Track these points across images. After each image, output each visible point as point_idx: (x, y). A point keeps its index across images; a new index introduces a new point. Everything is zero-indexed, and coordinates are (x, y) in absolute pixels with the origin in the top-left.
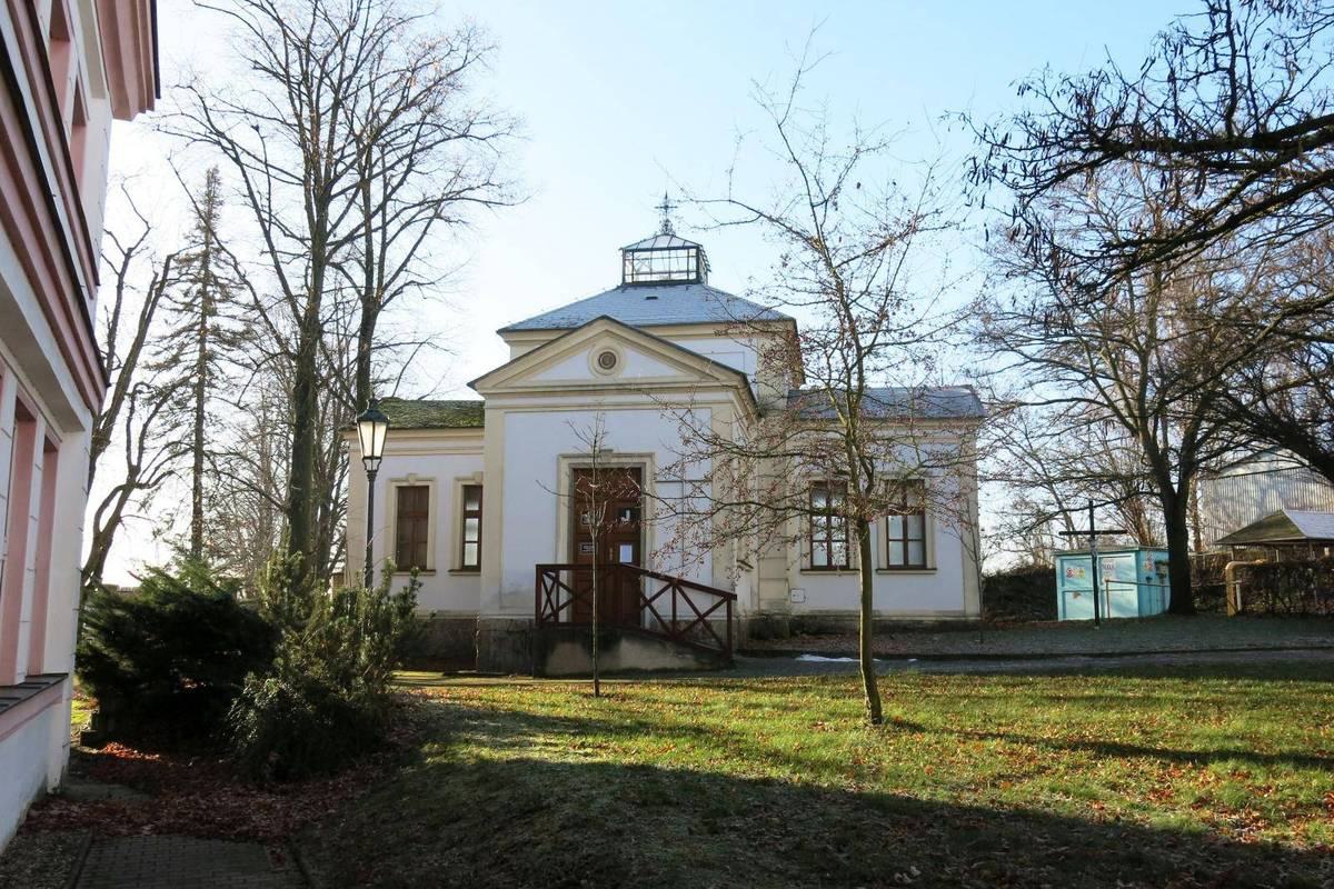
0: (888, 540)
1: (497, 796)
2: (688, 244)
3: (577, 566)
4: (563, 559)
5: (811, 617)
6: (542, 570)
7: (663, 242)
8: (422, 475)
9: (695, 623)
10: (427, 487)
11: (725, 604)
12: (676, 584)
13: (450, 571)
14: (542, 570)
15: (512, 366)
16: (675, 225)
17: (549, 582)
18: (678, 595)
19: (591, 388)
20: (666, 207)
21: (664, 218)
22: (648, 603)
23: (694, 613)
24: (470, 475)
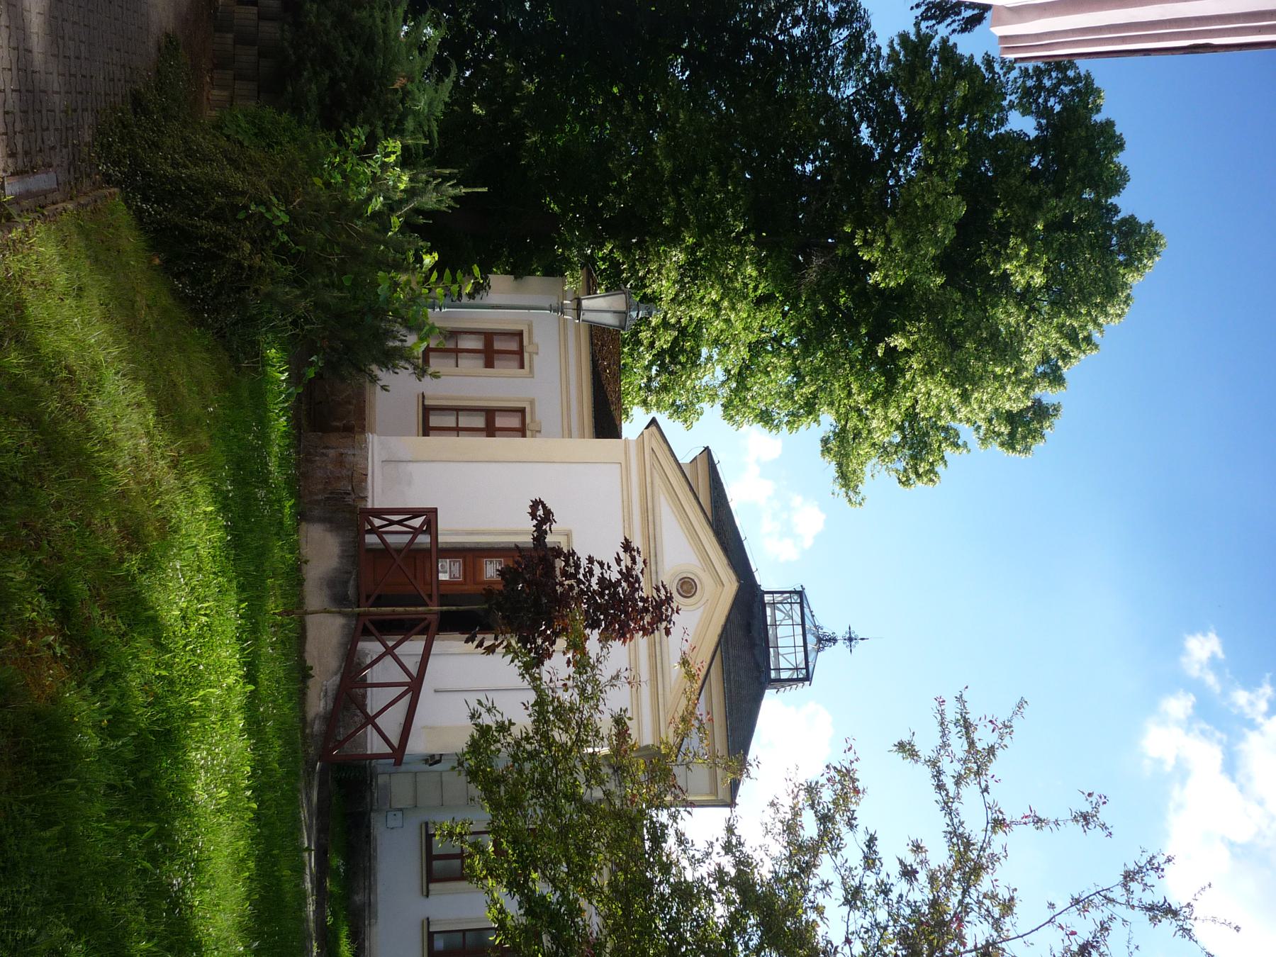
5: (368, 836)
7: (811, 640)
11: (389, 751)
12: (414, 686)
16: (829, 652)
17: (417, 522)
20: (850, 639)
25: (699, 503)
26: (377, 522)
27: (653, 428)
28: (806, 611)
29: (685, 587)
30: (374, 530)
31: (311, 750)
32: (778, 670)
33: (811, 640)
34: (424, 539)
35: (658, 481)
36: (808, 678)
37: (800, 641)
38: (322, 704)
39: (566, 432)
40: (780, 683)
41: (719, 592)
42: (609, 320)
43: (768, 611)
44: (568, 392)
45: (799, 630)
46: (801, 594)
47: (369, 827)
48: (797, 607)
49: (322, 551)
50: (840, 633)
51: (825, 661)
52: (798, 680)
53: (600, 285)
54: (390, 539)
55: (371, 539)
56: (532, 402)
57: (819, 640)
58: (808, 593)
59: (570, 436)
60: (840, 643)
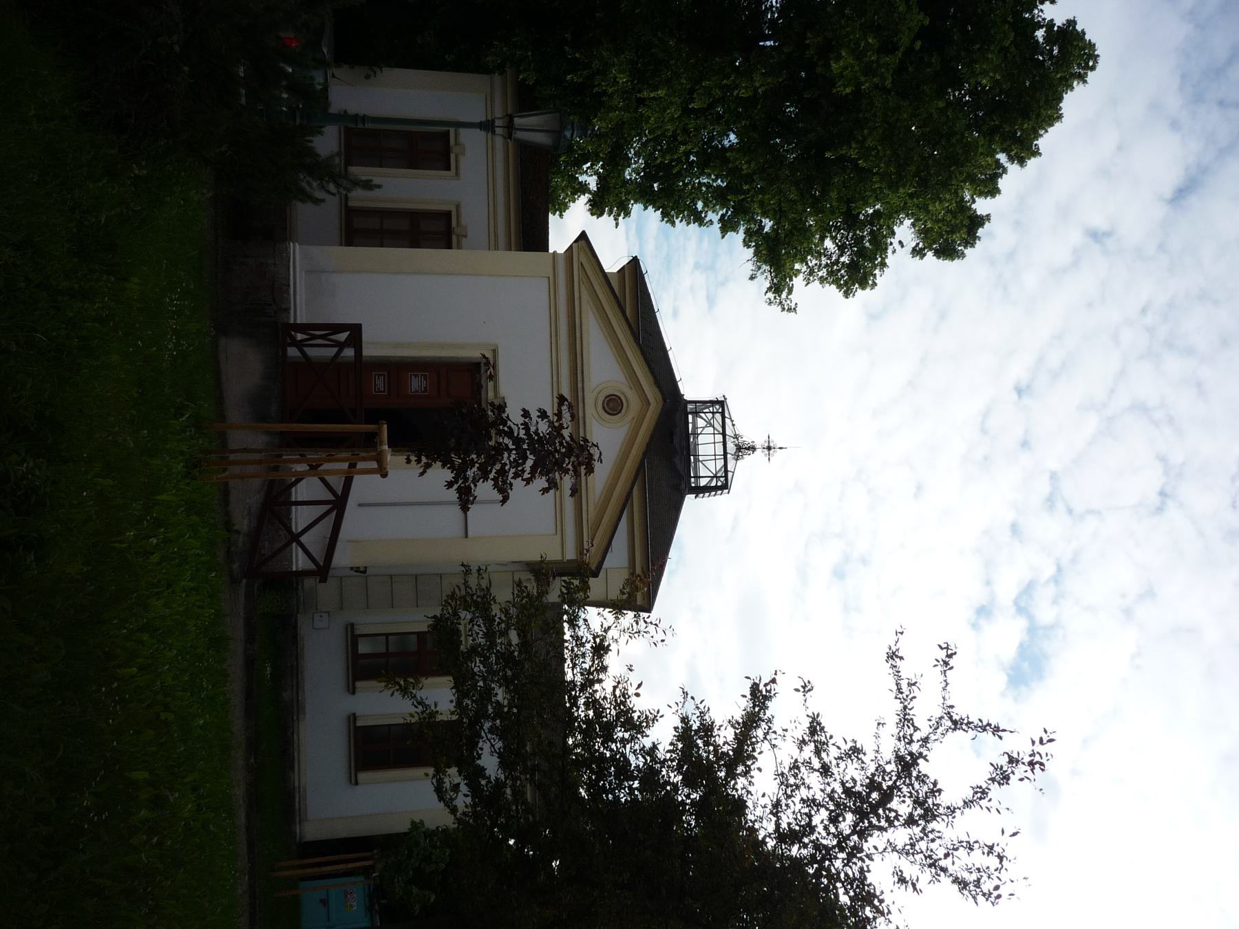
0: (387, 635)
1: (323, 201)
2: (730, 475)
3: (364, 367)
4: (367, 352)
6: (355, 331)
7: (731, 448)
8: (463, 162)
9: (289, 530)
10: (448, 168)
11: (312, 566)
12: (338, 504)
14: (355, 331)
15: (601, 275)
16: (748, 460)
17: (343, 337)
18: (326, 507)
19: (580, 385)
20: (769, 448)
21: (758, 444)
22: (296, 538)
23: (300, 530)
24: (463, 222)
25: (627, 320)
26: (300, 337)
27: (583, 242)
28: (727, 421)
29: (611, 404)
30: (296, 344)
32: (697, 477)
33: (731, 448)
34: (349, 353)
35: (586, 297)
36: (725, 487)
37: (720, 451)
38: (246, 522)
39: (492, 242)
40: (699, 491)
41: (643, 409)
42: (540, 138)
43: (690, 417)
44: (496, 235)
45: (719, 438)
46: (722, 403)
47: (295, 627)
48: (718, 416)
49: (243, 367)
50: (759, 442)
51: (744, 470)
52: (716, 488)
53: (510, 706)
54: (312, 352)
55: (292, 352)
56: (458, 207)
57: (739, 448)
58: (731, 404)
59: (496, 248)
60: (758, 452)
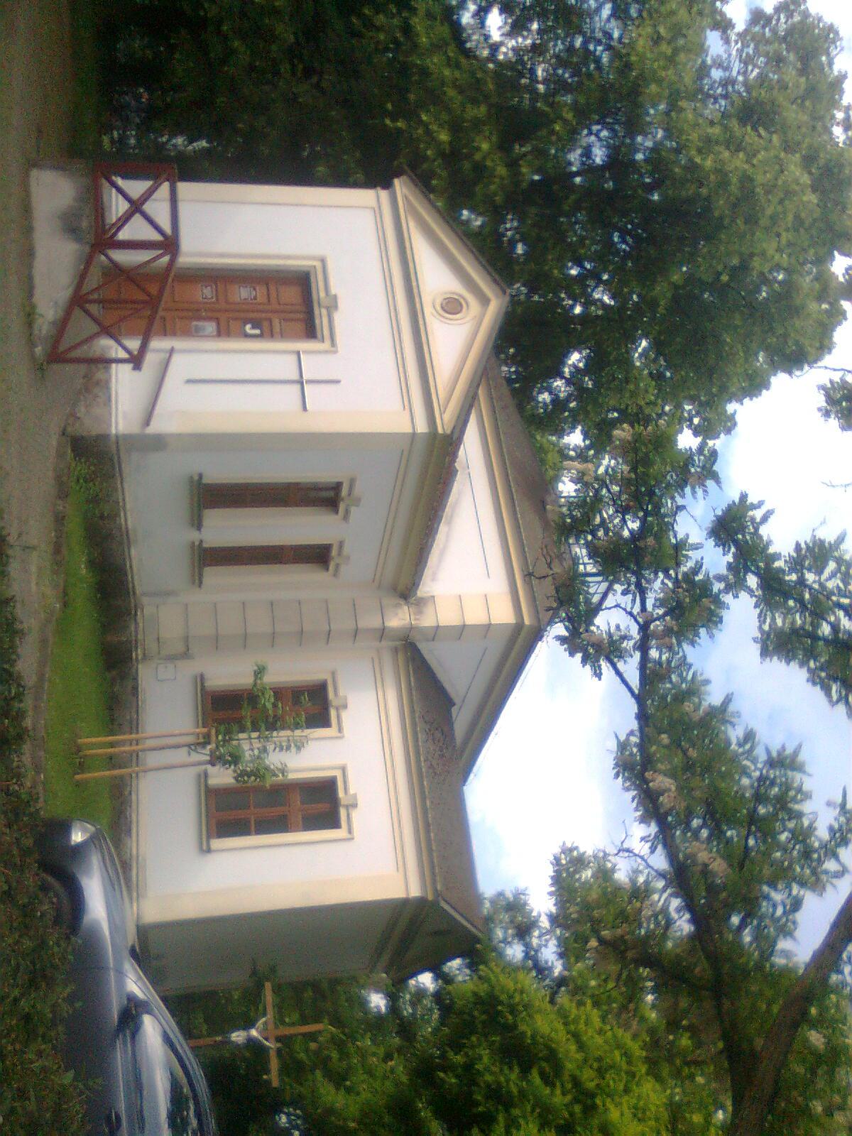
5: (135, 689)
13: (202, 677)
31: (38, 350)
47: (136, 679)
56: (323, 261)
